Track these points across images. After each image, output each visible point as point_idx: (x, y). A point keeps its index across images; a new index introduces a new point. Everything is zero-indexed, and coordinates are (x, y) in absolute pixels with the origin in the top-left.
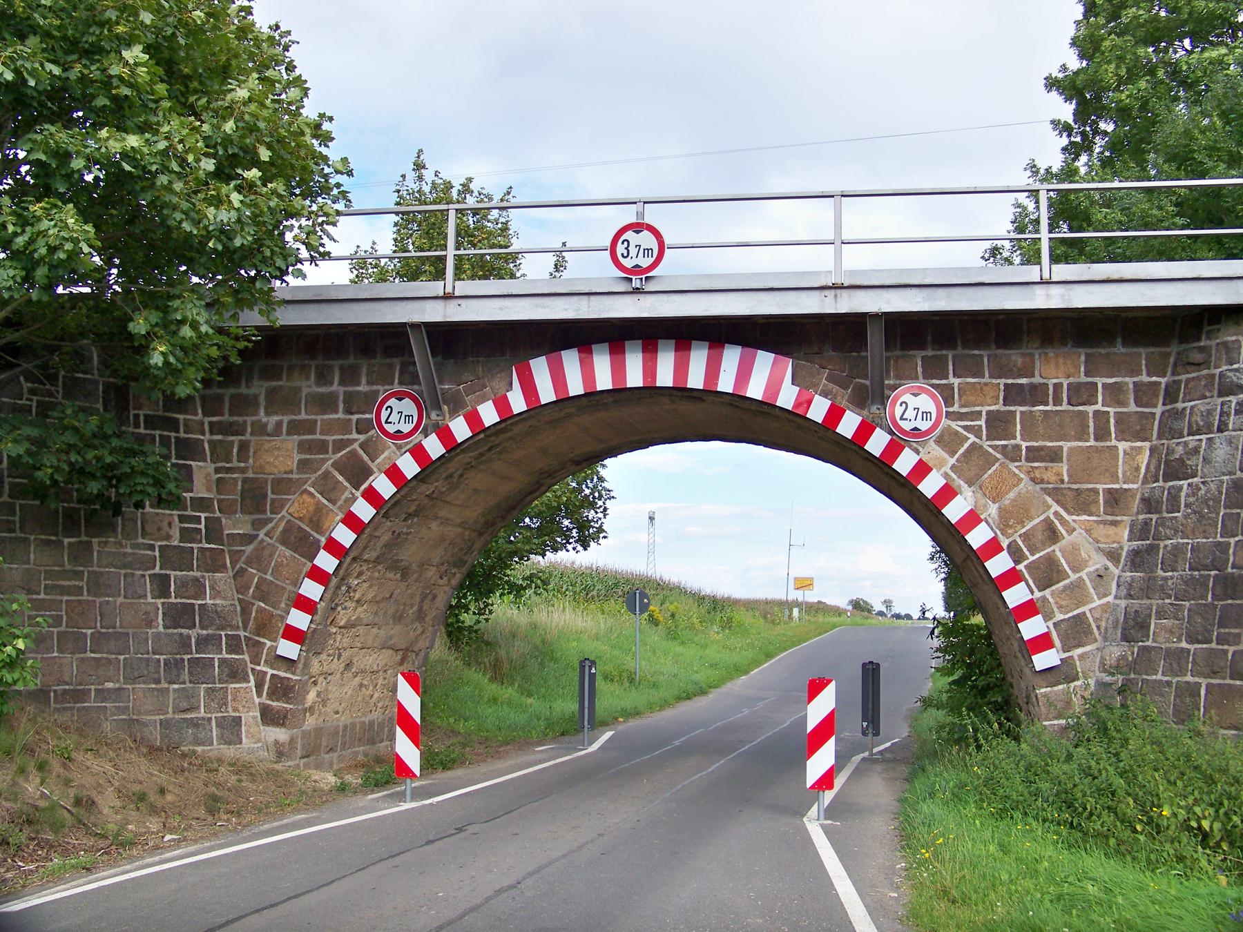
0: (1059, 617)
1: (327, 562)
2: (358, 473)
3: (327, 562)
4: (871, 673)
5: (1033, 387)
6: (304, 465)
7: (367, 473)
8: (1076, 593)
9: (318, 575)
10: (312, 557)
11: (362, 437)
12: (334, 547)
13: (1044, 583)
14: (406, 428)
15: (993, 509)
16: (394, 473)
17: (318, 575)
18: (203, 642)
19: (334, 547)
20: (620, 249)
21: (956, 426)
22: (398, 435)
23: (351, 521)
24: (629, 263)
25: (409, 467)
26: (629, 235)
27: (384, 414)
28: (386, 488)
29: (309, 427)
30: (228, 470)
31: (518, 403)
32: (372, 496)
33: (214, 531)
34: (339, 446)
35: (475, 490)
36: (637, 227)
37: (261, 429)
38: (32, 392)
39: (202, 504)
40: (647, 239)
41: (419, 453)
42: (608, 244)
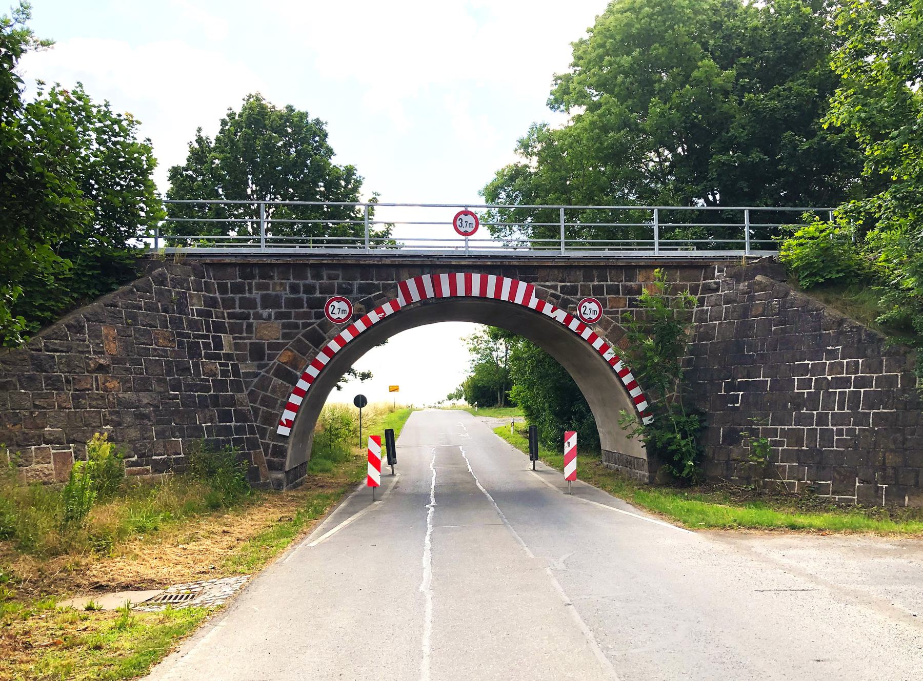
1: (303, 385)
6: (285, 336)
11: (319, 321)
12: (307, 378)
14: (343, 316)
17: (299, 392)
18: (239, 430)
20: (458, 223)
24: (462, 230)
26: (462, 216)
27: (330, 309)
30: (240, 338)
31: (401, 301)
33: (236, 372)
34: (306, 325)
37: (258, 317)
39: (228, 357)
40: (470, 219)
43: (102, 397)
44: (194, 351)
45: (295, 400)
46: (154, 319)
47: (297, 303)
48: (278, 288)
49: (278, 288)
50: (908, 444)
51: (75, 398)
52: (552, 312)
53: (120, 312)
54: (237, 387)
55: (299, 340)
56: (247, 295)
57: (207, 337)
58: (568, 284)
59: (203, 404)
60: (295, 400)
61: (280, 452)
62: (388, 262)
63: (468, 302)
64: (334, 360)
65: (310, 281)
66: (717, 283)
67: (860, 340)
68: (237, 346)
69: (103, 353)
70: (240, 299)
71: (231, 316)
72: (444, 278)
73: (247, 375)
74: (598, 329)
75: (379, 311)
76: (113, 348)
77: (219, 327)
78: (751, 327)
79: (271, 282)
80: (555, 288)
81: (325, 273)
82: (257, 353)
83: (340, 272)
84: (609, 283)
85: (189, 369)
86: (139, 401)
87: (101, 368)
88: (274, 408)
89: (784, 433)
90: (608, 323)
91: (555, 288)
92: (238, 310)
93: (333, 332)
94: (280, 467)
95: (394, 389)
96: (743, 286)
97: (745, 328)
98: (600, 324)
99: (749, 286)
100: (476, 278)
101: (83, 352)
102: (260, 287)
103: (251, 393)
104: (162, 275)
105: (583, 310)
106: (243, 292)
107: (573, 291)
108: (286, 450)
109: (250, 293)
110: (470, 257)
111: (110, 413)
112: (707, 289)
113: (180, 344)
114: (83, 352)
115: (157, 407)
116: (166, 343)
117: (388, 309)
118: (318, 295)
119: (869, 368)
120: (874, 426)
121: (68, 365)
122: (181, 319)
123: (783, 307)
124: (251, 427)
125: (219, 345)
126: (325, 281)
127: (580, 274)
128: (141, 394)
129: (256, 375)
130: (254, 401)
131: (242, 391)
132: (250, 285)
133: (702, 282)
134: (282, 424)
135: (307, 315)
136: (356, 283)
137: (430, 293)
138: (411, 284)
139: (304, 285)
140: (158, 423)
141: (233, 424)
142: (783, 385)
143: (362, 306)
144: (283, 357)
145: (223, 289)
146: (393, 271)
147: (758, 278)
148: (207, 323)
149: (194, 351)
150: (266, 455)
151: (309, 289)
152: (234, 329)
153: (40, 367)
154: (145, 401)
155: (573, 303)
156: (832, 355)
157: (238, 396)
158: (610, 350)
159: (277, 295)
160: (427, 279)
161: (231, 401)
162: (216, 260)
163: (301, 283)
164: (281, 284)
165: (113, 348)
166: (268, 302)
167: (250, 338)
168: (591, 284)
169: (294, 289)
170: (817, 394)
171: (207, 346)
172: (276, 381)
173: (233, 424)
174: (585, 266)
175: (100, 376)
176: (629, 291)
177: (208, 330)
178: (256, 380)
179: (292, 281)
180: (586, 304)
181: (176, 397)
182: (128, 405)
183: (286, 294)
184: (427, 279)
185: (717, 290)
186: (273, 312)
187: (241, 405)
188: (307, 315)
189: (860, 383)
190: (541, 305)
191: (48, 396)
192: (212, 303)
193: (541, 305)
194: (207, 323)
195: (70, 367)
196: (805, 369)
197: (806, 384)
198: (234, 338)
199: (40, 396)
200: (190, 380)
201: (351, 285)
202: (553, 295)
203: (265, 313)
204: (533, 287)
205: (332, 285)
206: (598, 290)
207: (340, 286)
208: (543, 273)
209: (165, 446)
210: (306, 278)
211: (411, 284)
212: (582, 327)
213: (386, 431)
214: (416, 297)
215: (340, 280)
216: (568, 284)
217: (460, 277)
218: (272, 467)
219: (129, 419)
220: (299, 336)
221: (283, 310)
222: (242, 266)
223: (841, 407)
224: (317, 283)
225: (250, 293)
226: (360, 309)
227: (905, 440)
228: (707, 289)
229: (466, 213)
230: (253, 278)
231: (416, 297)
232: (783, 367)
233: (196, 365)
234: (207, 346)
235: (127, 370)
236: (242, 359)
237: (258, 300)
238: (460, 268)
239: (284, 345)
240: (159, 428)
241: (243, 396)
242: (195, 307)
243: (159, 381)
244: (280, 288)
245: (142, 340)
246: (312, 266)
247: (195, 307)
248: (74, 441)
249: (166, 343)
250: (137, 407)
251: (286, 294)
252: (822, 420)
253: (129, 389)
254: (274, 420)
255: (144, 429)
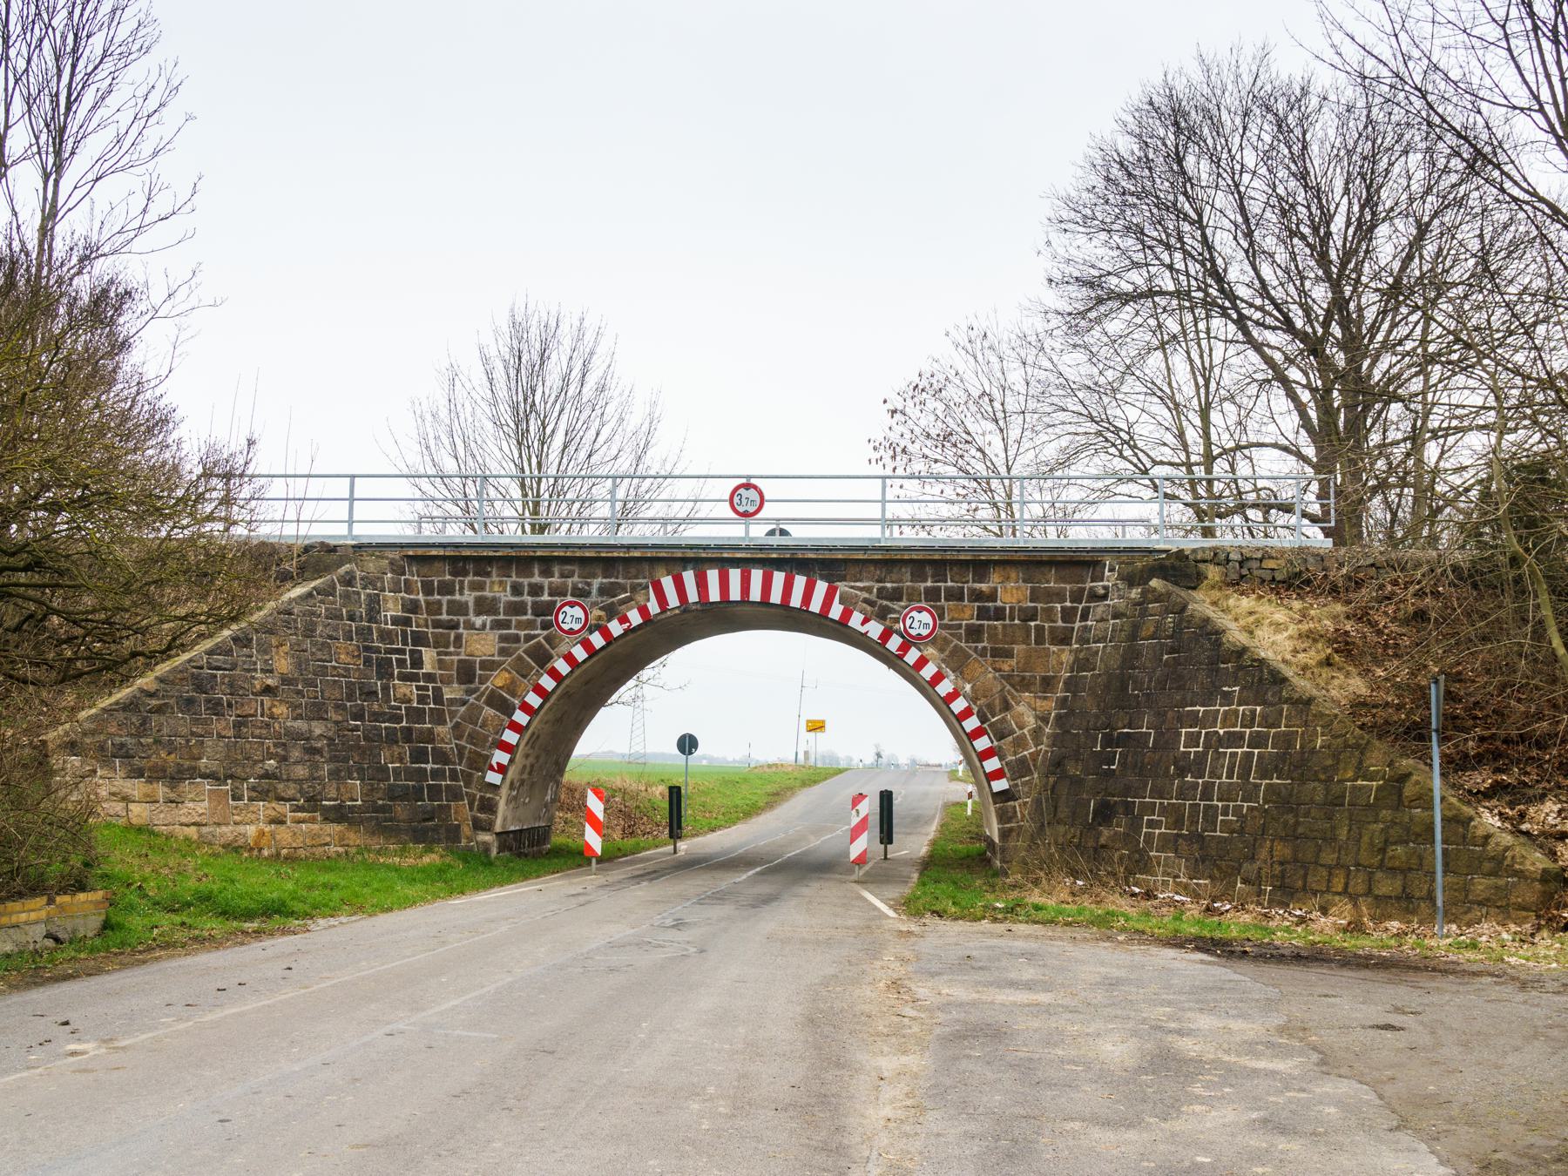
0: (1010, 758)
1: (521, 718)
2: (542, 657)
3: (521, 718)
4: (886, 798)
5: (996, 608)
6: (502, 652)
7: (549, 658)
8: (1020, 743)
9: (515, 727)
10: (510, 715)
11: (545, 633)
12: (526, 708)
13: (1001, 737)
14: (577, 627)
15: (968, 687)
16: (569, 658)
17: (515, 727)
18: (436, 774)
19: (526, 708)
20: (736, 499)
21: (944, 633)
22: (571, 632)
23: (539, 690)
24: (741, 509)
25: (580, 654)
26: (742, 491)
27: (561, 617)
28: (563, 667)
29: (507, 625)
30: (446, 654)
31: (653, 607)
32: (554, 673)
33: (438, 698)
34: (529, 638)
35: (82, 887)
36: (747, 486)
37: (470, 626)
38: (322, 602)
39: (430, 677)
40: (752, 494)
41: (586, 644)
42: (727, 497)
43: (268, 725)
44: (384, 669)
45: (510, 737)
46: (336, 629)
47: (517, 609)
48: (496, 588)
49: (496, 588)
50: (1300, 830)
51: (238, 725)
52: (863, 623)
53: (295, 621)
54: (439, 718)
55: (520, 658)
56: (457, 597)
57: (402, 652)
58: (889, 585)
59: (391, 738)
60: (510, 737)
61: (489, 807)
62: (637, 554)
63: (746, 608)
64: (563, 686)
65: (537, 579)
66: (1106, 588)
67: (1261, 679)
68: (441, 664)
69: (271, 671)
70: (449, 602)
71: (437, 624)
72: (713, 576)
73: (452, 702)
74: (930, 651)
75: (624, 619)
76: (283, 664)
77: (420, 639)
78: (1138, 655)
79: (488, 581)
80: (868, 590)
81: (556, 570)
82: (466, 673)
83: (576, 568)
84: (949, 584)
85: (376, 693)
86: (311, 731)
87: (268, 690)
88: (483, 747)
89: (1164, 810)
90: (946, 641)
91: (868, 590)
92: (444, 617)
93: (563, 649)
94: (488, 827)
95: (816, 727)
96: (1135, 593)
97: (1131, 657)
98: (934, 643)
99: (1143, 594)
100: (757, 575)
101: (248, 670)
102: (475, 587)
103: (457, 726)
104: (351, 574)
105: (908, 622)
106: (452, 593)
107: (896, 595)
108: (496, 805)
109: (461, 594)
110: (747, 548)
111: (275, 745)
112: (1095, 597)
113: (367, 661)
114: (248, 670)
115: (331, 739)
116: (349, 660)
117: (635, 618)
118: (546, 597)
119: (1268, 722)
120: (1266, 801)
121: (231, 685)
122: (370, 629)
123: (1178, 627)
124: (453, 772)
125: (417, 662)
126: (556, 580)
127: (907, 573)
128: (314, 723)
129: (464, 703)
130: (459, 737)
131: (444, 723)
132: (462, 583)
133: (1089, 585)
134: (491, 768)
135: (530, 625)
136: (596, 583)
137: (693, 596)
138: (668, 583)
139: (530, 585)
140: (332, 759)
141: (429, 767)
142: (1166, 741)
143: (602, 613)
144: (499, 679)
145: (428, 589)
146: (646, 567)
147: (1154, 583)
148: (404, 633)
149: (384, 669)
150: (471, 809)
151: (536, 590)
152: (441, 643)
153: (200, 688)
154: (318, 732)
155: (895, 611)
156: (1227, 698)
157: (439, 729)
158: (946, 681)
159: (494, 599)
160: (689, 577)
161: (430, 737)
162: (420, 552)
163: (526, 581)
164: (501, 583)
165: (283, 664)
166: (484, 606)
167: (458, 654)
168: (923, 585)
169: (517, 590)
170: (1205, 754)
171: (401, 663)
172: (489, 711)
173: (429, 767)
174: (911, 561)
175: (266, 700)
176: (977, 596)
177: (405, 643)
178: (463, 709)
179: (514, 578)
180: (914, 614)
181: (356, 728)
182: (296, 736)
183: (506, 596)
184: (689, 577)
185: (1105, 597)
186: (489, 619)
187: (442, 740)
188: (530, 625)
189: (1258, 741)
190: (847, 614)
191: (206, 722)
192: (413, 607)
193: (847, 614)
194: (404, 633)
195: (233, 688)
196: (1194, 720)
197: (1193, 740)
198: (439, 654)
199: (196, 722)
200: (376, 707)
201: (589, 584)
202: (866, 601)
203: (478, 621)
204: (836, 589)
205: (565, 584)
206: (932, 595)
207: (575, 588)
208: (853, 570)
209: (338, 789)
210: (532, 575)
211: (668, 583)
212: (905, 647)
213: (671, 788)
214: (673, 601)
215: (576, 579)
216: (889, 585)
217: (735, 575)
218: (478, 826)
219: (296, 754)
220: (520, 651)
221: (501, 617)
222: (453, 560)
223: (1230, 776)
224: (546, 582)
225: (461, 594)
226: (600, 618)
227: (1297, 823)
228: (1095, 597)
229: (747, 486)
230: (466, 574)
231: (673, 601)
232: (1170, 714)
233: (386, 689)
234: (401, 663)
235: (299, 692)
236: (447, 681)
237: (471, 604)
238: (735, 562)
239: (500, 664)
240: (332, 766)
241: (442, 730)
242: (392, 608)
243: (337, 707)
244: (499, 589)
245: (319, 655)
246: (541, 559)
247: (392, 608)
248: (232, 777)
249: (349, 660)
250: (307, 739)
251: (506, 596)
252: (1207, 795)
253: (299, 717)
254: (480, 763)
255: (315, 766)
